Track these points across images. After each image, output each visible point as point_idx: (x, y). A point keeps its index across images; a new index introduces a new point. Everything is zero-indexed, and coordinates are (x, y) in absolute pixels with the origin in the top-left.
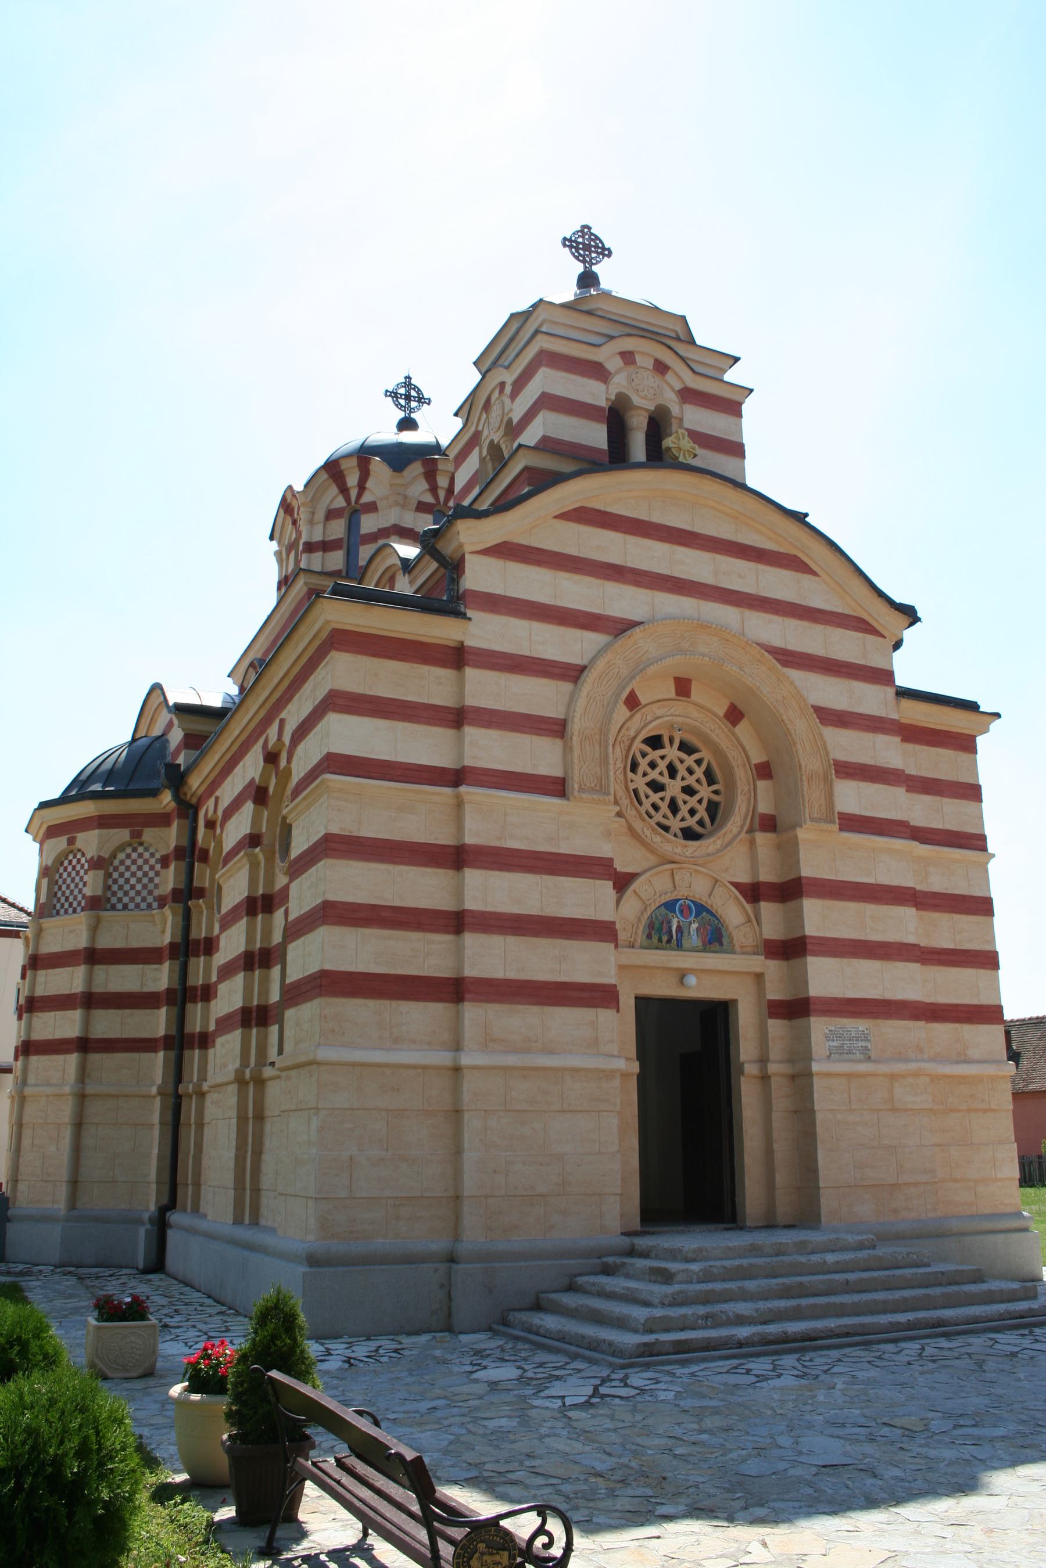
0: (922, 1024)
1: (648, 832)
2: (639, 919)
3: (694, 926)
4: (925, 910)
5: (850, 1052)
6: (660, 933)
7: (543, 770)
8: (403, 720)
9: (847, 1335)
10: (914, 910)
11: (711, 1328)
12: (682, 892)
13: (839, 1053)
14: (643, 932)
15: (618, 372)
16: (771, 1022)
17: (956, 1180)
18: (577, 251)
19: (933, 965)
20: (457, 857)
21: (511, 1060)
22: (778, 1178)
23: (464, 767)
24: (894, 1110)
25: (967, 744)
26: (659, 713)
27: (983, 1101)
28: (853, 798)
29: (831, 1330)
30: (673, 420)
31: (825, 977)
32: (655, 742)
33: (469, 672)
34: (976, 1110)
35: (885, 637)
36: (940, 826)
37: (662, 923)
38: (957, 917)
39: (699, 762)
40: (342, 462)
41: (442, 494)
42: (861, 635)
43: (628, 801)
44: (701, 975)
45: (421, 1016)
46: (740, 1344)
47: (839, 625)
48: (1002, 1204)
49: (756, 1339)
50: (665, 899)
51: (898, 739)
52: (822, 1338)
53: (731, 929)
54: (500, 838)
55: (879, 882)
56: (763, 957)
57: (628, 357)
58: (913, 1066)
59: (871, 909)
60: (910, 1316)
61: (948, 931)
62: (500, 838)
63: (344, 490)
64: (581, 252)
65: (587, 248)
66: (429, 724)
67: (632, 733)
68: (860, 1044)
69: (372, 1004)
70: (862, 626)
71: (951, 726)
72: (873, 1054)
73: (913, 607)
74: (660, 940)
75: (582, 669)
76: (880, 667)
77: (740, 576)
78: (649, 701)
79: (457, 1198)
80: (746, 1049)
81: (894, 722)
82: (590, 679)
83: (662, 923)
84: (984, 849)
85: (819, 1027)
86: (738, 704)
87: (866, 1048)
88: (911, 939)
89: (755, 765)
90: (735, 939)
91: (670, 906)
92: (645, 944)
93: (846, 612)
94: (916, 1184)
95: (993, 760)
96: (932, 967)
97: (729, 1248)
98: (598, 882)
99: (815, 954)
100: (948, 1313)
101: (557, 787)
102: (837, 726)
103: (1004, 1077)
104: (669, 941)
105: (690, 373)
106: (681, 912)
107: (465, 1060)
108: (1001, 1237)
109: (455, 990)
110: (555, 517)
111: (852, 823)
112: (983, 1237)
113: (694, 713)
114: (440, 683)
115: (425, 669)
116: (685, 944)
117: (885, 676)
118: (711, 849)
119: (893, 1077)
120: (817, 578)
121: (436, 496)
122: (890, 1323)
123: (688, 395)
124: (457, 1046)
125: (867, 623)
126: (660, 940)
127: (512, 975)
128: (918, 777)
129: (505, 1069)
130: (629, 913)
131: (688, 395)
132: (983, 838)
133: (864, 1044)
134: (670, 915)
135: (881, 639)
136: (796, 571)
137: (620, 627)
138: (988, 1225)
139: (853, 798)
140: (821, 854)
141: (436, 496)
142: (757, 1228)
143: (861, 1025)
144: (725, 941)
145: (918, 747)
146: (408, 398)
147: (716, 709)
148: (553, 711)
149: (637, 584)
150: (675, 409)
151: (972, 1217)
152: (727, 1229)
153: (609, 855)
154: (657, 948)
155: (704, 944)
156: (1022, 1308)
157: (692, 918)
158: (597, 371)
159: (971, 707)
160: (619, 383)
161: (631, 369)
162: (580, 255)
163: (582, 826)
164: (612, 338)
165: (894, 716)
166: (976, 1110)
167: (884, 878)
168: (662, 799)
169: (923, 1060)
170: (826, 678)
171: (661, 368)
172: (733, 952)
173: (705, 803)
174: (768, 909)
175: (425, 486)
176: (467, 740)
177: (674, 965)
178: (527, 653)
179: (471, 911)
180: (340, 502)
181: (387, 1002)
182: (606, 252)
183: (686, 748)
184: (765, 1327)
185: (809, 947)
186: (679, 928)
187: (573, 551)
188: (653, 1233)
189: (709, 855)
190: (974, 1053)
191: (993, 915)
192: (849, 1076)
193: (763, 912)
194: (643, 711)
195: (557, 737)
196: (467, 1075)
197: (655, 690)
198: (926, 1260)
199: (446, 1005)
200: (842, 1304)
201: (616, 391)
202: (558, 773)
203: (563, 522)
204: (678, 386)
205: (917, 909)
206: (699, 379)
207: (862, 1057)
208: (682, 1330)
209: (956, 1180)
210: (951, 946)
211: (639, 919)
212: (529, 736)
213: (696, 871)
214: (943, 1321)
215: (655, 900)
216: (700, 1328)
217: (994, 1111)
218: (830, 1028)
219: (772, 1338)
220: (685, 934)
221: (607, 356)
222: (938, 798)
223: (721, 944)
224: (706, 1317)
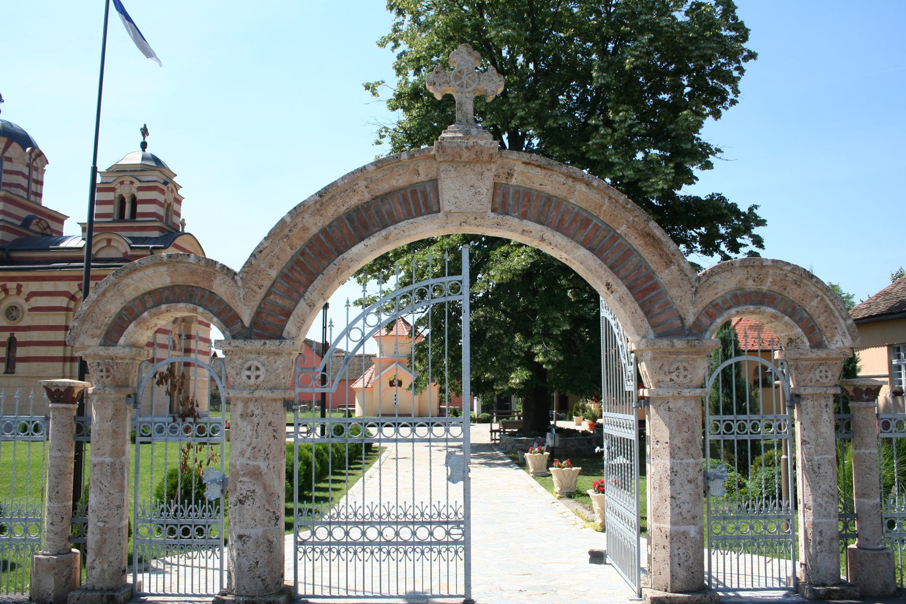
85: (192, 369)
123: (140, 189)
158: (113, 190)
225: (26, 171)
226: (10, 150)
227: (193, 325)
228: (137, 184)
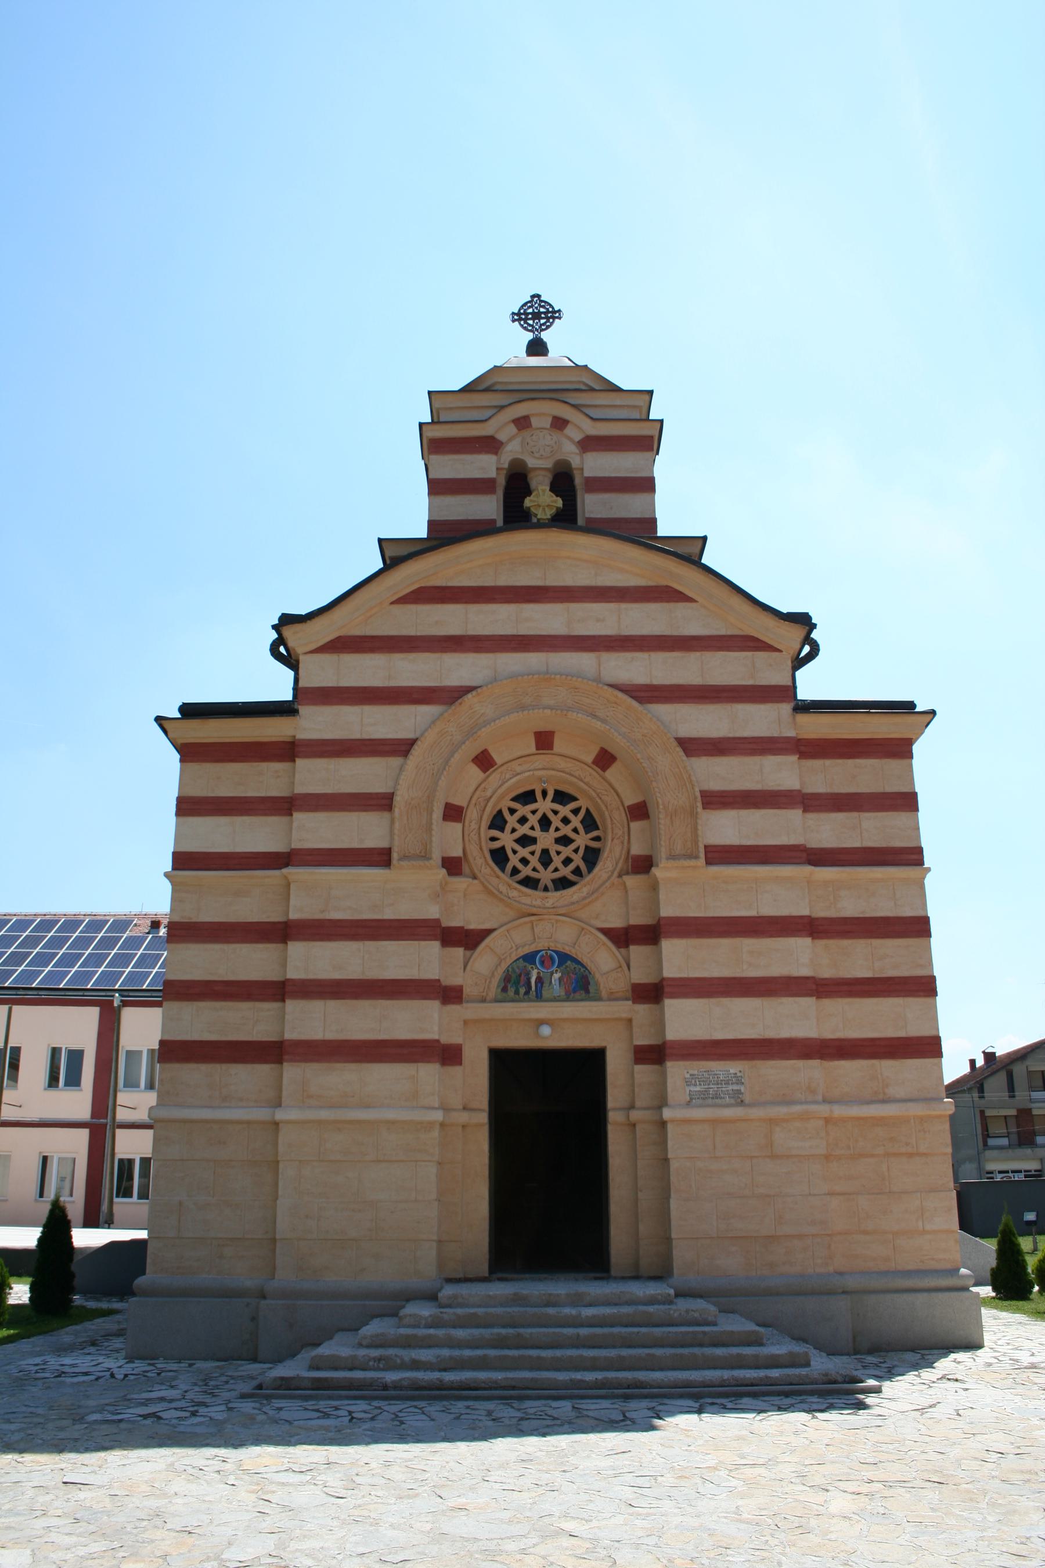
0: (815, 1063)
1: (503, 888)
2: (493, 974)
3: (557, 976)
5: (716, 1096)
6: (517, 983)
7: (370, 843)
8: (242, 815)
9: (514, 1388)
10: (809, 940)
11: (383, 1370)
12: (541, 945)
13: (704, 1099)
14: (498, 986)
15: (510, 440)
16: (638, 1068)
17: (866, 1232)
18: (525, 322)
19: (841, 997)
20: (282, 932)
21: (324, 1114)
22: (641, 1227)
23: (293, 850)
24: (774, 1157)
25: (901, 749)
26: (518, 769)
28: (727, 828)
29: (496, 1382)
30: (575, 472)
31: (684, 1019)
32: (527, 797)
33: (300, 762)
34: (895, 1155)
36: (857, 845)
37: (520, 975)
38: (876, 942)
39: (576, 812)
42: (750, 654)
43: (482, 861)
44: (555, 1024)
45: (245, 1077)
46: (385, 1387)
47: (720, 649)
48: (933, 1259)
49: (405, 1383)
50: (527, 950)
51: (794, 758)
52: (485, 1389)
53: (597, 976)
54: (323, 912)
55: (761, 914)
56: (630, 1002)
57: (523, 423)
58: (797, 1108)
59: (748, 944)
60: (599, 1375)
61: (884, 957)
62: (323, 912)
64: (531, 322)
65: (536, 316)
66: (266, 815)
67: (489, 793)
68: (730, 1087)
69: (204, 1068)
70: (751, 644)
71: (887, 731)
72: (747, 1099)
73: (807, 614)
74: (517, 992)
75: (411, 743)
77: (598, 620)
78: (506, 760)
79: (274, 1240)
80: (615, 1096)
81: (788, 739)
82: (416, 751)
83: (520, 975)
84: (921, 863)
86: (606, 747)
87: (739, 1092)
88: (805, 972)
89: (629, 807)
90: (602, 985)
91: (529, 958)
92: (499, 997)
93: (729, 633)
94: (800, 1237)
95: (930, 765)
96: (840, 1000)
97: (489, 1296)
98: (423, 943)
99: (673, 996)
100: (642, 1376)
101: (382, 858)
102: (712, 755)
103: (939, 1117)
104: (527, 993)
105: (589, 421)
106: (542, 963)
107: (280, 1115)
108: (921, 1298)
109: (273, 1052)
110: (392, 603)
111: (721, 855)
113: (562, 764)
114: (278, 777)
115: (264, 766)
116: (545, 994)
117: (789, 691)
118: (575, 898)
119: (772, 1122)
120: (693, 605)
122: (571, 1380)
123: (590, 444)
124: (278, 1104)
125: (757, 640)
126: (517, 992)
127: (330, 1036)
128: (827, 794)
129: (320, 1122)
130: (485, 965)
131: (590, 444)
132: (919, 851)
133: (735, 1087)
134: (529, 967)
135: (777, 654)
136: (668, 601)
137: (450, 696)
139: (727, 828)
140: (685, 890)
142: (623, 1278)
143: (734, 1067)
144: (592, 988)
145: (828, 762)
147: (583, 757)
148: (379, 787)
149: (478, 650)
150: (575, 461)
152: (596, 1279)
153: (436, 916)
154: (513, 1001)
155: (568, 993)
156: (748, 1376)
157: (555, 968)
158: (490, 445)
159: (908, 707)
160: (513, 450)
161: (526, 433)
162: (529, 325)
163: (409, 891)
164: (502, 408)
165: (791, 733)
166: (895, 1155)
167: (769, 908)
168: (533, 853)
169: (816, 1102)
170: (701, 706)
171: (559, 423)
172: (599, 999)
173: (581, 852)
174: (637, 951)
176: (295, 825)
177: (527, 1016)
178: (358, 736)
179: (292, 980)
181: (218, 1066)
182: (552, 315)
183: (562, 797)
184: (444, 1374)
185: (666, 990)
186: (539, 980)
187: (411, 632)
188: (512, 1280)
189: (573, 903)
190: (893, 1091)
191: (930, 936)
192: (714, 1122)
193: (632, 956)
194: (500, 770)
195: (385, 810)
197: (513, 750)
198: (710, 1319)
199: (273, 1065)
200: (571, 1357)
201: (510, 458)
202: (383, 844)
203: (401, 606)
204: (578, 437)
205: (813, 938)
206: (599, 424)
207: (732, 1101)
208: (351, 1369)
209: (866, 1232)
210: (869, 974)
211: (493, 974)
212: (357, 813)
213: (557, 921)
214: (642, 1382)
215: (510, 954)
216: (370, 1369)
217: (924, 1154)
218: (691, 1072)
219: (424, 1384)
220: (546, 985)
221: (500, 427)
222: (855, 814)
223: (587, 991)
224: (379, 1359)
228: (582, 426)
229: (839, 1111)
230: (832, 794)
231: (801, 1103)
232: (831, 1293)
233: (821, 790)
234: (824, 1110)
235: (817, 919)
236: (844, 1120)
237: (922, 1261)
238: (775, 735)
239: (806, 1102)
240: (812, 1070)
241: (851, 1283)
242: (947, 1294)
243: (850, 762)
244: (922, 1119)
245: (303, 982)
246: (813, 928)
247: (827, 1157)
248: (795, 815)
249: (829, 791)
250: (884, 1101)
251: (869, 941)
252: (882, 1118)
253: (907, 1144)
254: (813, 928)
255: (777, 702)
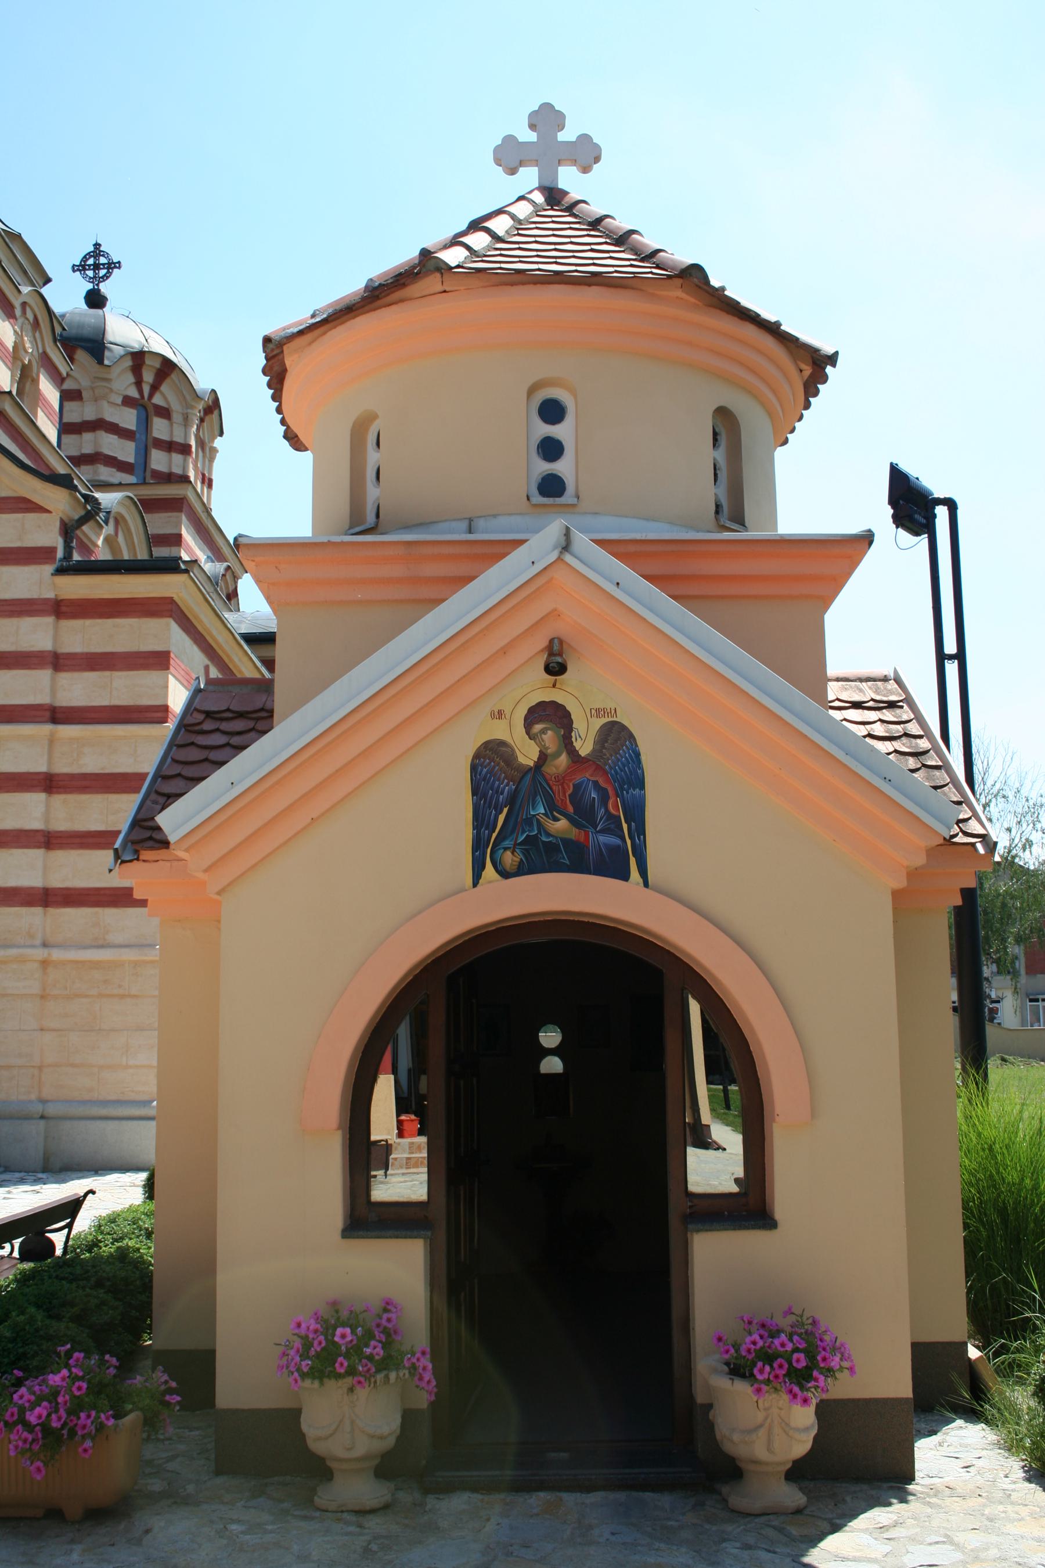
4: (70, 792)
17: (73, 1065)
19: (72, 848)
27: (120, 986)
35: (49, 512)
36: (106, 703)
38: (113, 797)
40: (147, 356)
41: (146, 389)
63: (139, 383)
76: (39, 545)
81: (46, 601)
88: (37, 825)
94: (8, 1067)
108: (111, 1125)
112: (88, 1122)
121: (141, 391)
128: (82, 654)
135: (45, 515)
138: (80, 1111)
141: (141, 391)
145: (88, 622)
146: (96, 267)
151: (84, 1102)
165: (51, 595)
169: (33, 946)
175: (131, 379)
180: (133, 393)
196: (405, 1124)
209: (73, 1065)
222: (107, 673)
225: (128, 419)
226: (164, 388)
227: (805, 1498)
229: (56, 955)
230: (87, 654)
231: (18, 947)
232: (28, 1117)
233: (78, 649)
234: (40, 953)
235: (58, 775)
236: (64, 963)
237: (123, 1093)
238: (35, 597)
239: (25, 946)
240: (32, 917)
241: (51, 1110)
242: (135, 1122)
243: (110, 622)
244: (136, 964)
245: (72, 777)
246: (50, 783)
247: (42, 997)
248: (44, 676)
249: (86, 650)
250: (102, 947)
251: (106, 796)
252: (99, 962)
253: (120, 986)
254: (50, 783)
255: (40, 563)
